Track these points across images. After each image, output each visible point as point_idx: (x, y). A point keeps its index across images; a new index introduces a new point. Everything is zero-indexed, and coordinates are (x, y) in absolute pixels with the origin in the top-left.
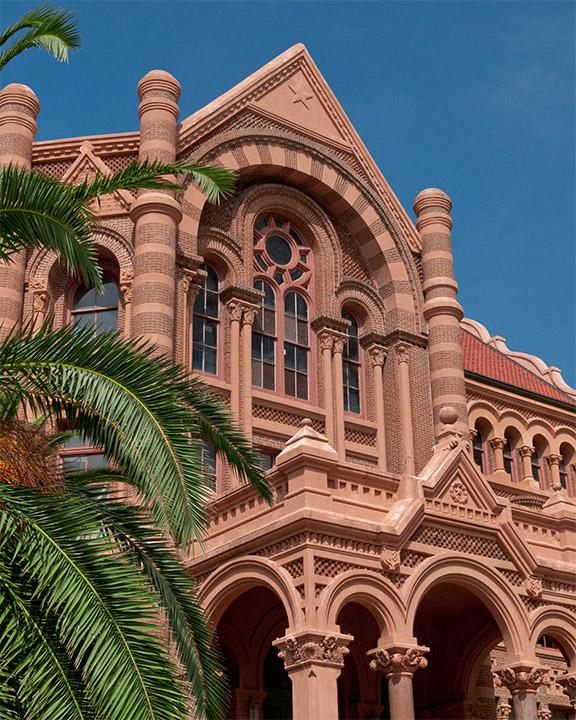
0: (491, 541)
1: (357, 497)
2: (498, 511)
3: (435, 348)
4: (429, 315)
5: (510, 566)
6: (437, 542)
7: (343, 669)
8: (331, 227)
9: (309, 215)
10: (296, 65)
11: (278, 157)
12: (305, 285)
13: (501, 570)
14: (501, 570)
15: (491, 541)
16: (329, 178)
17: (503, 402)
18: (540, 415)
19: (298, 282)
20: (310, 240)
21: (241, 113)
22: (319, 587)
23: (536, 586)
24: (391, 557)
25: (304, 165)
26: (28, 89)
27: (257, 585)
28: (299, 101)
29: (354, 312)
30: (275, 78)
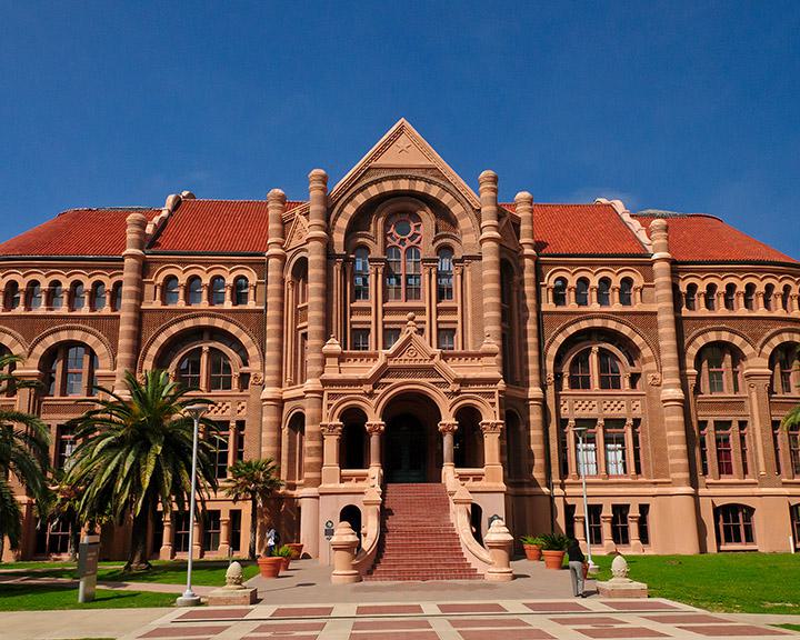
0: (429, 371)
1: (357, 364)
2: (433, 357)
3: (484, 260)
4: (481, 242)
5: (442, 380)
6: (398, 377)
7: (506, 494)
8: (428, 210)
9: (415, 207)
10: (401, 131)
11: (388, 186)
12: (419, 242)
13: (434, 383)
14: (434, 383)
15: (429, 371)
16: (420, 187)
17: (593, 265)
18: (624, 265)
19: (413, 243)
20: (419, 219)
21: (368, 170)
22: (329, 405)
23: (456, 387)
24: (368, 388)
25: (404, 185)
26: (277, 190)
27: (479, 443)
28: (407, 150)
29: (445, 250)
30: (386, 145)
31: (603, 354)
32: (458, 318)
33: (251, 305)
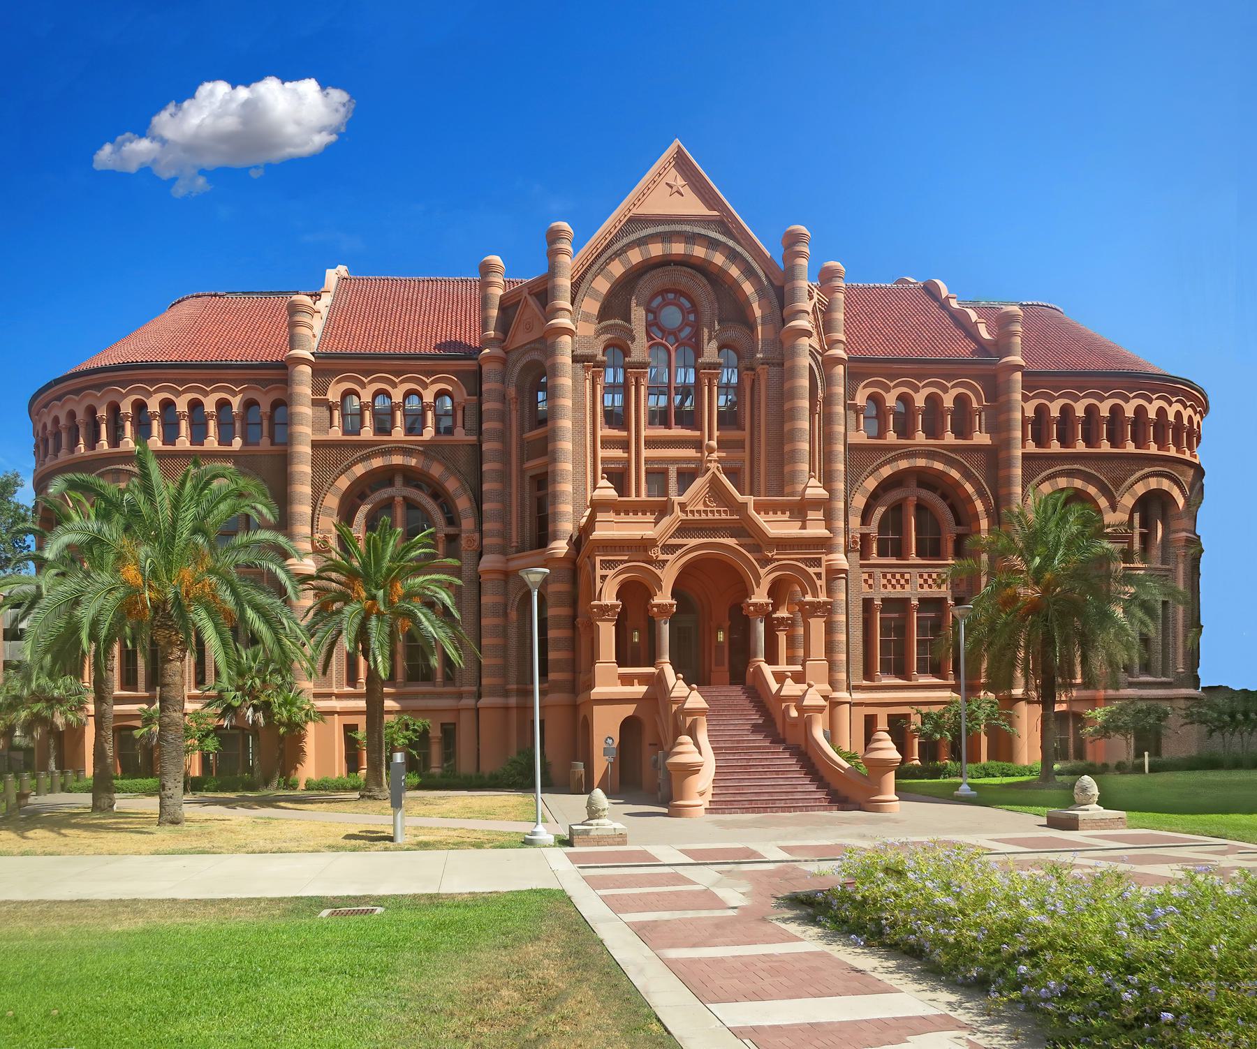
31: (921, 508)
32: (746, 455)
33: (460, 435)
